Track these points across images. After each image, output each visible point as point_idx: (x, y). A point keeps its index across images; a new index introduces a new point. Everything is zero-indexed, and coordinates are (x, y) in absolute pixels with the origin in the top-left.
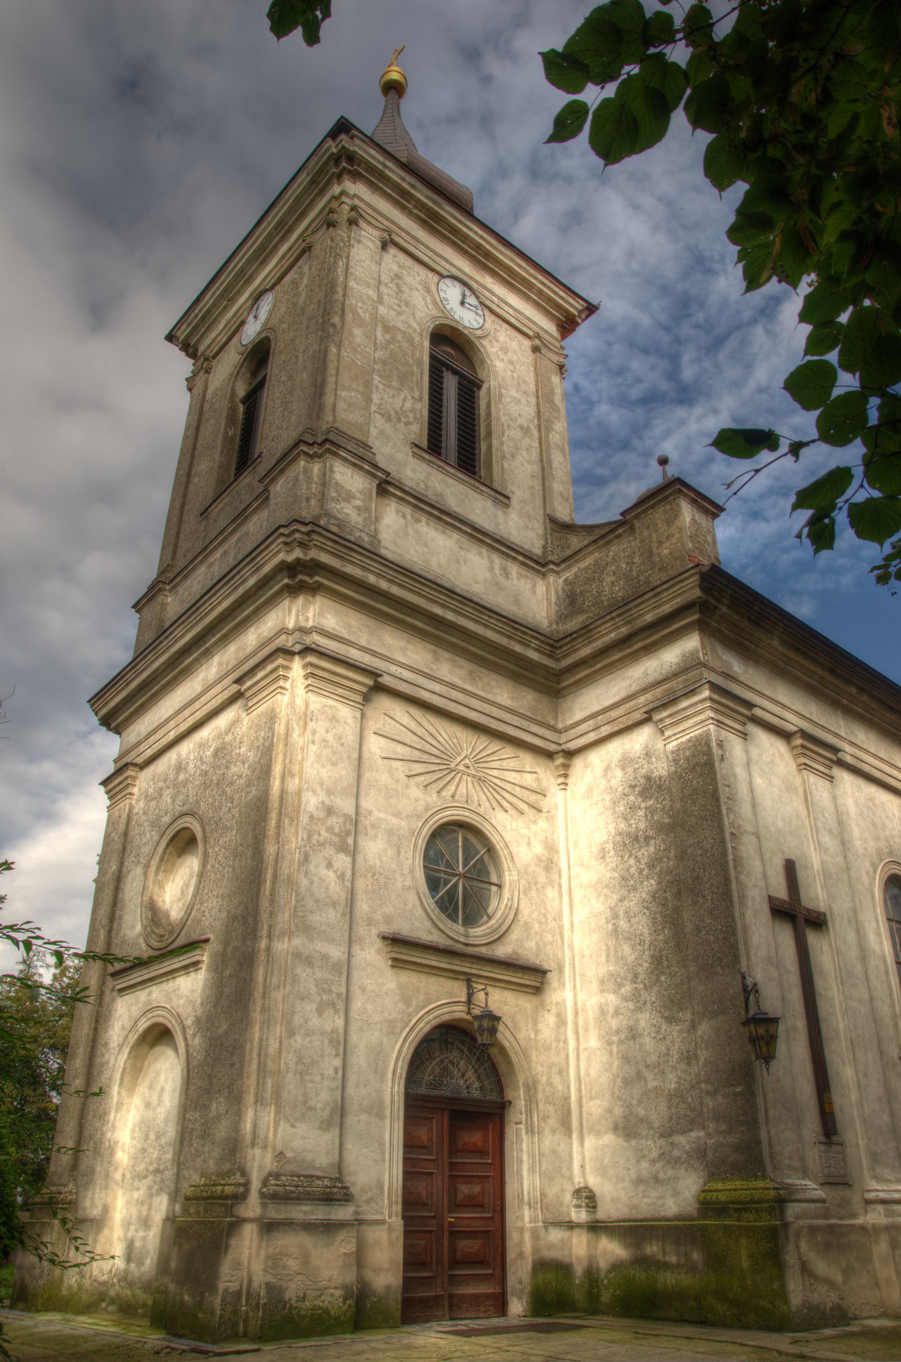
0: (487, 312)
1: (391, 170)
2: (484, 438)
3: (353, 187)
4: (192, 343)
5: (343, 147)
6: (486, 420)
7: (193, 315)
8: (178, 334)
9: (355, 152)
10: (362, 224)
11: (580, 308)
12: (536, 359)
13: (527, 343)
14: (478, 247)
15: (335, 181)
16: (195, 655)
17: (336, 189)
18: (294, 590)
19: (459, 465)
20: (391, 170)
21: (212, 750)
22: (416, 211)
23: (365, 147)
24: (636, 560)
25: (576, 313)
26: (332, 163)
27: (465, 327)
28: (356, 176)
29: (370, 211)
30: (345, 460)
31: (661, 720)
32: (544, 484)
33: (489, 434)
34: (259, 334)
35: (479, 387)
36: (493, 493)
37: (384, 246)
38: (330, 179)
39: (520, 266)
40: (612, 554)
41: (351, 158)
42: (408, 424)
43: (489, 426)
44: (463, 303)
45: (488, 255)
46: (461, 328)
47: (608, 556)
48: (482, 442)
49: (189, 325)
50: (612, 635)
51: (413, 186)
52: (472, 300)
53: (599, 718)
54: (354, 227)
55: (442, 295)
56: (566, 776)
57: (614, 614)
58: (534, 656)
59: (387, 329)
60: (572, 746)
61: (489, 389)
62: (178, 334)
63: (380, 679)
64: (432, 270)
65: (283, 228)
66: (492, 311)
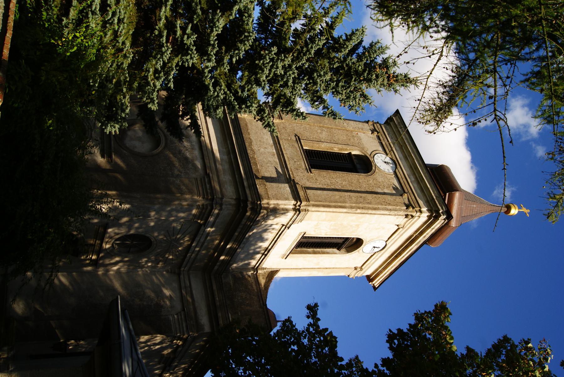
0: (372, 254)
1: (431, 231)
2: (314, 250)
3: (425, 216)
4: (391, 123)
5: (441, 216)
6: (322, 252)
7: (402, 126)
8: (397, 117)
9: (438, 219)
10: (406, 219)
11: (375, 285)
12: (352, 268)
13: (360, 265)
14: (400, 254)
15: (430, 209)
16: (230, 147)
17: (424, 209)
18: (238, 199)
19: (301, 243)
20: (431, 231)
21: (189, 156)
22: (415, 236)
23: (441, 224)
24: (248, 308)
25: (373, 283)
26: (437, 209)
27: (363, 248)
28: (429, 217)
29: (413, 221)
30: (293, 217)
31: (181, 315)
32: (294, 269)
33: (315, 253)
34: (375, 165)
35: (338, 249)
36: (287, 254)
37: (398, 226)
38: (431, 207)
39: (392, 267)
40: (254, 297)
41: (437, 218)
42: (315, 231)
43: (319, 253)
44: (374, 247)
45: (397, 257)
46: (362, 246)
47: (253, 295)
48: (312, 249)
49: (399, 123)
50: (217, 299)
51: (425, 237)
52: (376, 250)
53: (189, 289)
54: (405, 217)
55: (377, 241)
56: (171, 272)
57: (224, 301)
58: (216, 268)
59: (358, 226)
60: (182, 276)
61: (335, 254)
62: (397, 117)
63: (203, 226)
64: (389, 239)
65: (420, 180)
66: (372, 256)
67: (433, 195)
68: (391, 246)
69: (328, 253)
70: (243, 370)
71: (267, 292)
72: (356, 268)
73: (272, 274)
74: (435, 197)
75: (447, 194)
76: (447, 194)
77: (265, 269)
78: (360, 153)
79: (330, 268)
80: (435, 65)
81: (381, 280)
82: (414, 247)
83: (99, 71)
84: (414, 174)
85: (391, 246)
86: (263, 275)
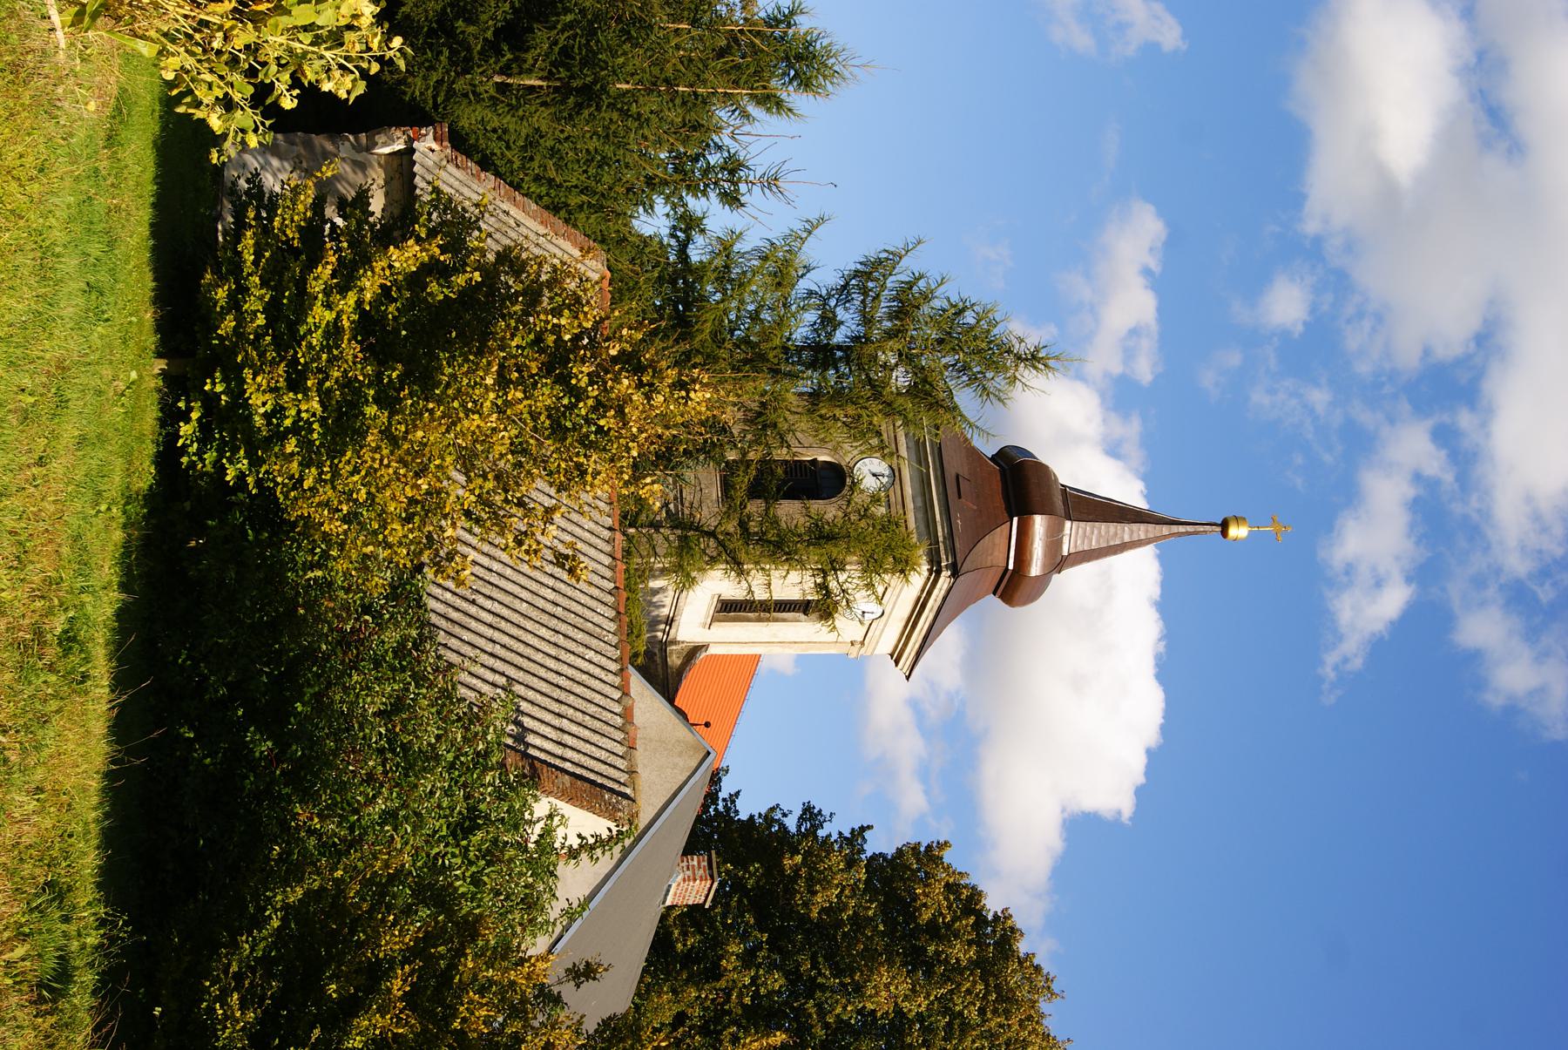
33: (759, 620)
61: (798, 621)
67: (940, 534)
68: (892, 610)
69: (784, 620)
70: (218, 396)
71: (680, 681)
72: (852, 644)
73: (694, 651)
74: (941, 539)
75: (1015, 520)
76: (1015, 520)
77: (683, 642)
78: (833, 460)
79: (802, 643)
80: (543, 610)
81: (908, 663)
82: (928, 615)
83: (437, 392)
84: (924, 495)
85: (892, 610)
86: (679, 653)
